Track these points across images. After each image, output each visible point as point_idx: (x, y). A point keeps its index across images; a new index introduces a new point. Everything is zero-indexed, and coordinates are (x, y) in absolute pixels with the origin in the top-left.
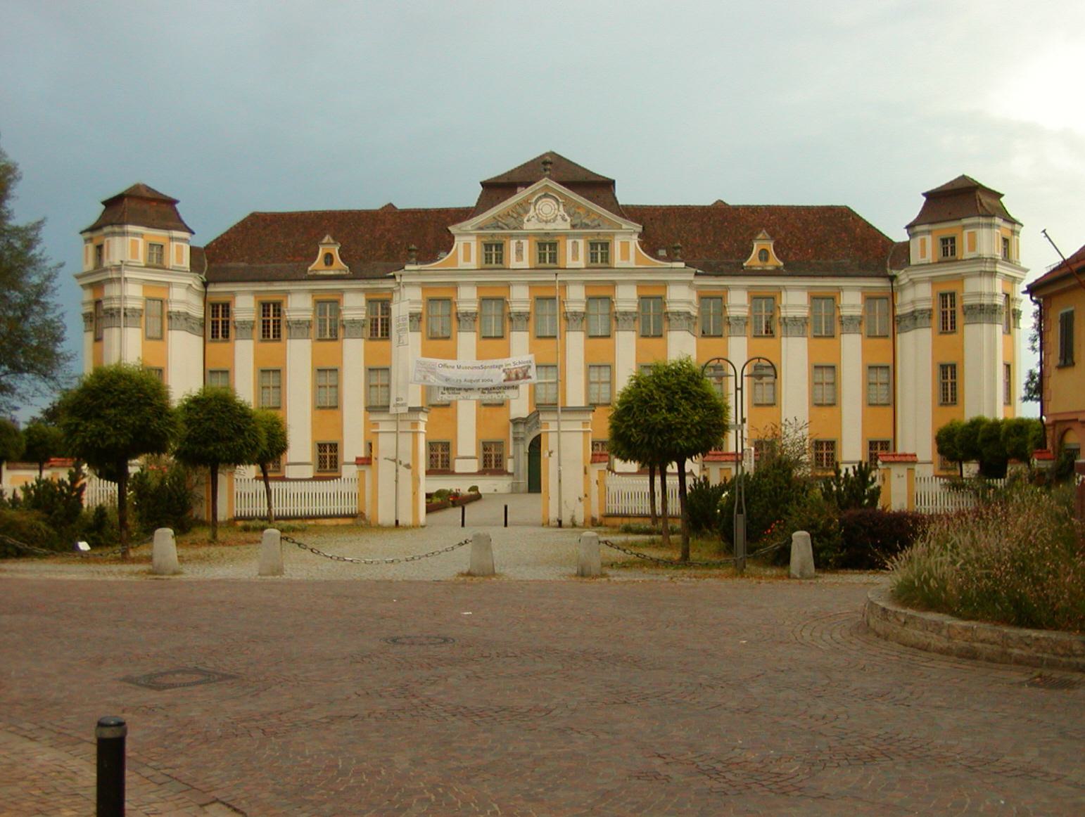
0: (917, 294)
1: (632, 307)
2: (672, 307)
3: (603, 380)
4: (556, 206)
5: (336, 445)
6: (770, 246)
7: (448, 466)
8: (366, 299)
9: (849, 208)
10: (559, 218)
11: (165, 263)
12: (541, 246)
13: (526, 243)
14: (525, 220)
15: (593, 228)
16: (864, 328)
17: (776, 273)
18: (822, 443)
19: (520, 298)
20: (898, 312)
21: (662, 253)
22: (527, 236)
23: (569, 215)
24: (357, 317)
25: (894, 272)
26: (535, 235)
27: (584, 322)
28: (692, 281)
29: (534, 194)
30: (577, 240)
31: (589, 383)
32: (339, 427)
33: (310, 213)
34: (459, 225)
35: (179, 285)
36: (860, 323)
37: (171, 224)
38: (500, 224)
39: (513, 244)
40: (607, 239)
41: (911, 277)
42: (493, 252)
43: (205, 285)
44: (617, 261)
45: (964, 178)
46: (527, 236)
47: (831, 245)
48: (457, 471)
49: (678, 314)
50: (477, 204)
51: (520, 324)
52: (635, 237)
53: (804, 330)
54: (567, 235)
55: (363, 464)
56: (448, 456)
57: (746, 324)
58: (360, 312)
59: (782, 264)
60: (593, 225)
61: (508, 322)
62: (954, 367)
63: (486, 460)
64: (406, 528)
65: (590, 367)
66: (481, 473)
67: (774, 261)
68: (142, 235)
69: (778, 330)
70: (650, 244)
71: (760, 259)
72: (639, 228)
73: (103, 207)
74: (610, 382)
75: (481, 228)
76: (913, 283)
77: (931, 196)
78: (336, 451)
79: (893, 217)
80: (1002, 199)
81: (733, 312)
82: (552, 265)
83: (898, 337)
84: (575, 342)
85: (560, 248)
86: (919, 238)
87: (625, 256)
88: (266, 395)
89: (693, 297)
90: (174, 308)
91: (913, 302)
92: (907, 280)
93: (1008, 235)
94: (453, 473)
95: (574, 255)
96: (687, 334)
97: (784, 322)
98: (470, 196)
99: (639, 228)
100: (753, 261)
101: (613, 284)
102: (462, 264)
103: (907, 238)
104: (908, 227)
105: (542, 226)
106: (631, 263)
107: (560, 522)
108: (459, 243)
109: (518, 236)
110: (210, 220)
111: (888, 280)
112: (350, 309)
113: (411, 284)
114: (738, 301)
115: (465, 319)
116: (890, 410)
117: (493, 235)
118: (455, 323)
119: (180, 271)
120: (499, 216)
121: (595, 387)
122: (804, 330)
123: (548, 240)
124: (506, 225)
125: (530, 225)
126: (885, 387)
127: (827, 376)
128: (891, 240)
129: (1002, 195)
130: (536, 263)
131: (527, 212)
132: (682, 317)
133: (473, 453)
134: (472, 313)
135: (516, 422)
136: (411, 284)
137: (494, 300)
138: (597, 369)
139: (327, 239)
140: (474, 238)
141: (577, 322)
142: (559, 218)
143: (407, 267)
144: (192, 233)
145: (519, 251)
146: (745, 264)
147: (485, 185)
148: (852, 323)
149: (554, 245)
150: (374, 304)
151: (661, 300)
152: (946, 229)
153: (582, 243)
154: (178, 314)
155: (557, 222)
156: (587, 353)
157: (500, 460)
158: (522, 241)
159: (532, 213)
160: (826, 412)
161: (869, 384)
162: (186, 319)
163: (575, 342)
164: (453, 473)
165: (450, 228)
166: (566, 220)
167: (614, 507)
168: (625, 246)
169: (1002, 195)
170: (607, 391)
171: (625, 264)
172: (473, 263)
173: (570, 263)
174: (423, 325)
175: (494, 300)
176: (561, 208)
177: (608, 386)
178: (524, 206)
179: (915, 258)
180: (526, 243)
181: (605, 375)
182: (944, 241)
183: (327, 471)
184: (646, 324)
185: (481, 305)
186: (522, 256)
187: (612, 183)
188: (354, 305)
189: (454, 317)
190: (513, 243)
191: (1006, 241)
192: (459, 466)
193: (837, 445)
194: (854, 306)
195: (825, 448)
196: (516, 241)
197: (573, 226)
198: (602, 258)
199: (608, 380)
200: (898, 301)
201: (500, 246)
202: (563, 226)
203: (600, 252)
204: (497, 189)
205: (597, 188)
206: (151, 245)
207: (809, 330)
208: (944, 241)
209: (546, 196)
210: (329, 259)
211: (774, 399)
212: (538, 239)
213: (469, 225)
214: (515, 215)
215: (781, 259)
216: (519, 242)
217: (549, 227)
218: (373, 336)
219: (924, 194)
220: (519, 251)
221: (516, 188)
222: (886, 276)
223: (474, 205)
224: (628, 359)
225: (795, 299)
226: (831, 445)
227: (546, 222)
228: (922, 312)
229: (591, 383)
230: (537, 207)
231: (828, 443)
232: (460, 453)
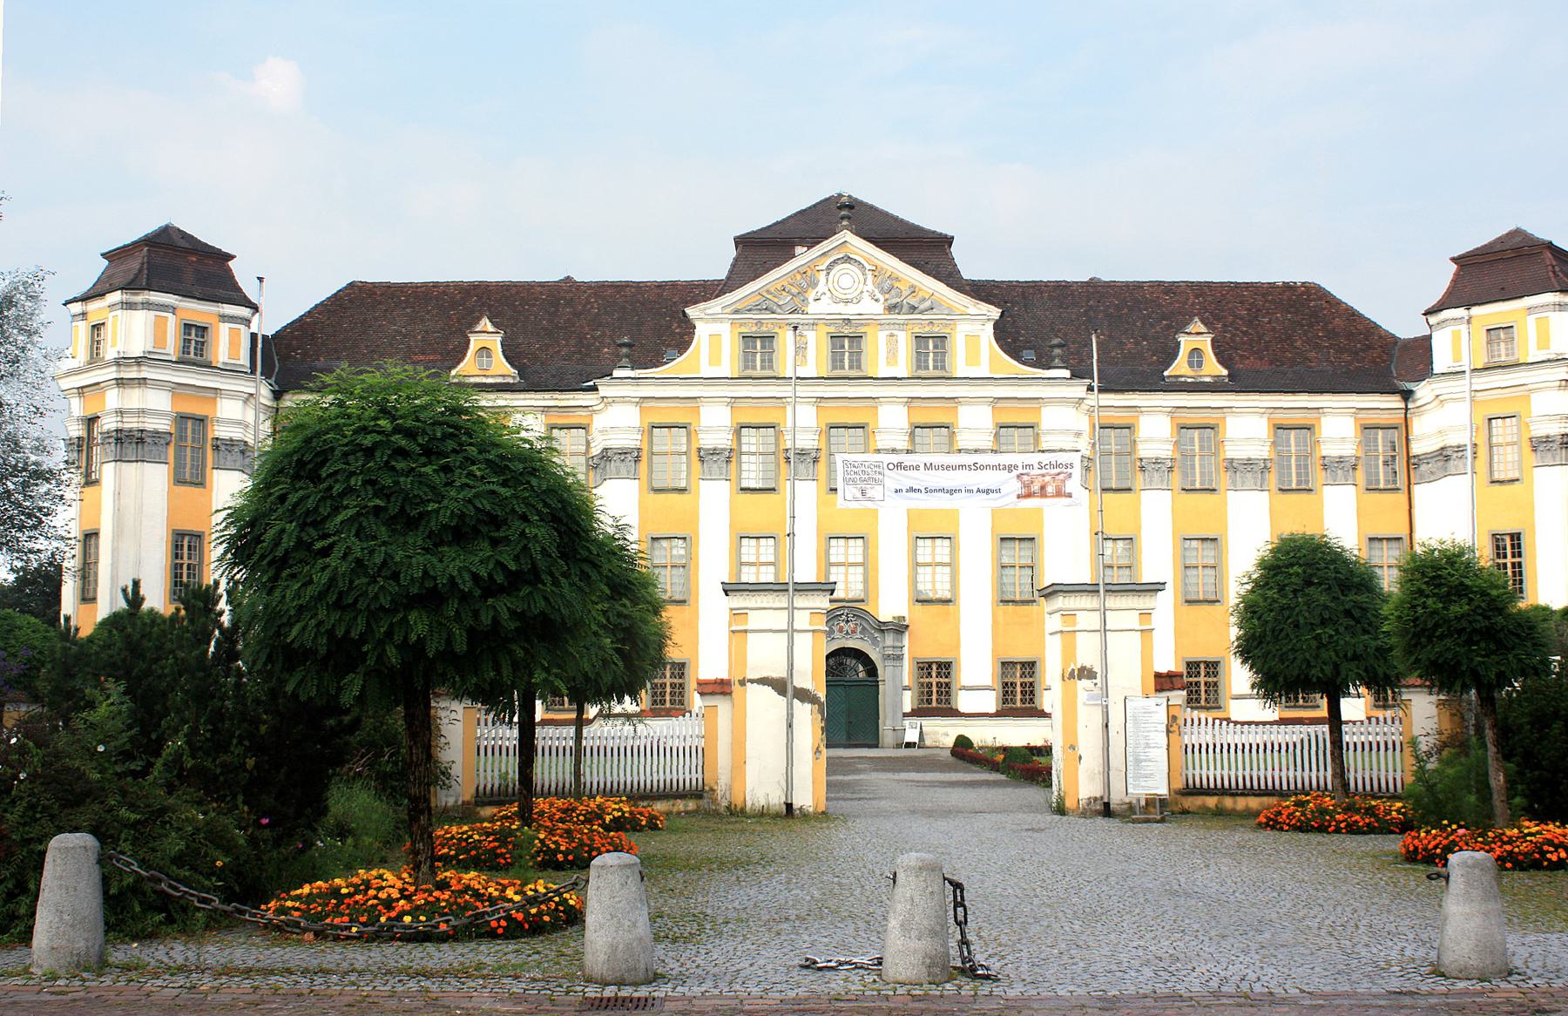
5: (1032, 664)
6: (1205, 342)
9: (1318, 289)
10: (866, 295)
11: (209, 356)
13: (811, 336)
14: (811, 299)
16: (1272, 479)
17: (1215, 387)
20: (1417, 448)
21: (1029, 355)
23: (882, 292)
25: (1410, 386)
26: (828, 323)
27: (733, 465)
33: (447, 285)
34: (702, 305)
35: (233, 395)
36: (1354, 468)
37: (221, 292)
42: (758, 344)
43: (277, 395)
45: (1517, 232)
47: (1298, 343)
48: (962, 710)
50: (731, 272)
51: (801, 467)
52: (990, 327)
53: (1263, 480)
55: (712, 694)
59: (1225, 372)
60: (922, 307)
62: (1516, 537)
63: (1007, 690)
64: (805, 816)
67: (1213, 368)
68: (174, 310)
70: (1009, 338)
71: (1191, 364)
72: (995, 313)
73: (1454, 267)
74: (742, 564)
75: (736, 312)
77: (1465, 262)
78: (682, 676)
80: (231, 263)
81: (1145, 451)
82: (767, 373)
83: (1417, 490)
85: (867, 345)
87: (973, 359)
88: (1192, 580)
89: (1082, 422)
90: (223, 432)
95: (889, 352)
97: (1232, 466)
98: (718, 265)
99: (995, 313)
100: (1180, 367)
105: (841, 308)
107: (1107, 805)
108: (702, 331)
110: (284, 293)
113: (623, 400)
117: (759, 322)
119: (231, 371)
122: (1263, 480)
123: (846, 331)
125: (820, 306)
127: (1206, 555)
128: (1393, 336)
129: (233, 257)
131: (814, 284)
136: (623, 400)
139: (485, 324)
142: (866, 295)
143: (616, 373)
144: (255, 308)
145: (800, 349)
146: (1166, 373)
147: (743, 242)
148: (1338, 468)
149: (856, 339)
154: (231, 443)
157: (1030, 691)
159: (821, 288)
162: (242, 452)
164: (955, 713)
165: (688, 310)
167: (1209, 771)
168: (972, 339)
169: (233, 257)
170: (947, 578)
177: (860, 569)
178: (808, 279)
179: (1440, 362)
181: (942, 550)
187: (948, 241)
189: (695, 458)
192: (964, 702)
193: (1220, 669)
197: (891, 308)
202: (872, 307)
203: (932, 348)
204: (762, 249)
205: (925, 249)
206: (188, 327)
207: (1272, 479)
211: (866, 590)
212: (832, 329)
213: (715, 306)
214: (794, 291)
215: (1226, 367)
217: (850, 310)
219: (1453, 259)
220: (800, 349)
221: (793, 247)
222: (1393, 391)
224: (1250, 532)
226: (945, 667)
229: (949, 565)
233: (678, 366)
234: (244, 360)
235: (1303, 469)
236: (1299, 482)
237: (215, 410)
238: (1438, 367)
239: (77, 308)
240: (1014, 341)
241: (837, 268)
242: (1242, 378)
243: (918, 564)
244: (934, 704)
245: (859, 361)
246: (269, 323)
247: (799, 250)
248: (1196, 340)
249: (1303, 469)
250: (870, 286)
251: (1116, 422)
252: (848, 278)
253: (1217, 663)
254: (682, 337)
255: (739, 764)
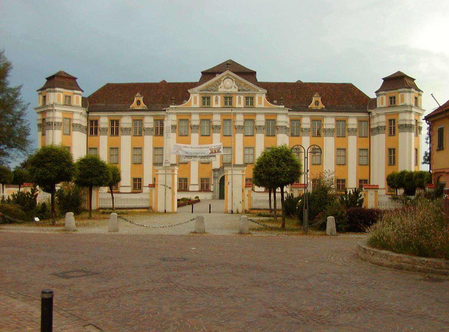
0: (380, 119)
1: (263, 124)
2: (279, 124)
3: (250, 153)
4: (232, 82)
6: (319, 99)
7: (186, 188)
8: (154, 119)
9: (352, 84)
10: (233, 87)
12: (226, 98)
13: (219, 97)
14: (219, 88)
15: (247, 91)
17: (322, 110)
18: (136, 179)
19: (217, 119)
20: (372, 127)
21: (275, 102)
22: (220, 94)
23: (237, 86)
24: (150, 127)
26: (223, 94)
28: (287, 113)
29: (223, 77)
30: (241, 96)
31: (244, 155)
32: (142, 171)
35: (77, 113)
36: (356, 131)
37: (74, 87)
38: (209, 89)
39: (214, 97)
40: (253, 96)
41: (377, 113)
42: (206, 100)
43: (88, 113)
44: (257, 105)
46: (220, 94)
48: (190, 190)
49: (282, 127)
50: (200, 81)
51: (216, 130)
52: (264, 95)
53: (333, 134)
54: (236, 94)
56: (187, 184)
57: (309, 131)
58: (198, 122)
59: (324, 107)
60: (247, 90)
61: (212, 129)
62: (394, 150)
63: (202, 186)
64: (169, 213)
65: (245, 148)
66: (200, 191)
67: (321, 106)
68: (62, 92)
69: (322, 134)
70: (270, 98)
71: (316, 105)
74: (253, 154)
75: (201, 91)
76: (378, 115)
77: (386, 80)
78: (141, 181)
79: (370, 88)
81: (304, 126)
83: (372, 137)
84: (239, 138)
86: (380, 97)
87: (260, 102)
89: (288, 120)
90: (75, 122)
91: (378, 123)
92: (375, 114)
93: (417, 96)
94: (189, 191)
95: (239, 102)
96: (285, 135)
99: (266, 91)
100: (312, 105)
101: (255, 114)
102: (193, 105)
103: (376, 97)
104: (376, 92)
106: (263, 106)
107: (232, 211)
108: (192, 97)
109: (216, 94)
110: (90, 86)
111: (367, 114)
112: (147, 123)
113: (172, 113)
114: (306, 122)
115: (194, 128)
116: (368, 167)
117: (206, 94)
118: (190, 129)
119: (78, 107)
120: (208, 86)
121: (247, 156)
122: (333, 134)
123: (228, 96)
124: (211, 89)
125: (221, 90)
126: (366, 158)
127: (342, 153)
129: (415, 80)
130: (223, 105)
131: (220, 84)
132: (283, 128)
133: (197, 183)
134: (197, 126)
135: (214, 170)
136: (172, 113)
137: (206, 120)
138: (248, 149)
139: (138, 94)
140: (198, 95)
141: (240, 129)
142: (233, 87)
143: (171, 106)
145: (217, 100)
148: (353, 131)
149: (231, 98)
150: (157, 121)
151: (274, 121)
152: (392, 93)
153: (242, 97)
154: (77, 124)
155: (232, 88)
156: (244, 143)
157: (208, 186)
158: (218, 96)
159: (222, 85)
160: (341, 168)
161: (359, 156)
162: (80, 127)
163: (239, 138)
164: (189, 191)
165: (188, 91)
166: (236, 88)
167: (254, 206)
168: (260, 98)
169: (415, 80)
170: (252, 158)
171: (260, 106)
172: (198, 105)
173: (237, 105)
174: (221, 130)
175: (206, 120)
176: (234, 82)
178: (219, 82)
179: (379, 105)
180: (219, 97)
181: (251, 151)
182: (391, 98)
183: (137, 190)
184: (268, 131)
185: (244, 123)
186: (218, 102)
188: (149, 122)
190: (214, 97)
191: (416, 98)
192: (191, 188)
194: (353, 124)
195: (341, 182)
196: (215, 96)
197: (239, 90)
198: (250, 103)
199: (252, 153)
200: (372, 122)
201: (209, 98)
202: (235, 90)
203: (250, 101)
204: (208, 75)
205: (249, 75)
206: (66, 96)
208: (391, 98)
209: (228, 78)
210: (139, 103)
213: (196, 89)
214: (215, 86)
215: (324, 105)
216: (216, 97)
217: (229, 91)
218: (156, 134)
219: (383, 79)
220: (217, 100)
223: (198, 81)
225: (329, 121)
226: (344, 181)
227: (228, 88)
228: (381, 127)
229: (246, 155)
230: (224, 82)
231: (342, 180)
232: (191, 183)
233: (186, 103)
234: (80, 104)
235: (344, 132)
236: (342, 135)
237: (73, 117)
238: (377, 107)
239: (40, 92)
240: (272, 98)
241: (225, 81)
242: (329, 109)
243: (253, 154)
244: (183, 189)
245: (231, 103)
246: (87, 94)
247: (217, 75)
248: (316, 98)
249: (344, 132)
250: (234, 84)
251: (296, 119)
252: (228, 84)
253: (345, 180)
254: (187, 97)
255: (156, 202)
